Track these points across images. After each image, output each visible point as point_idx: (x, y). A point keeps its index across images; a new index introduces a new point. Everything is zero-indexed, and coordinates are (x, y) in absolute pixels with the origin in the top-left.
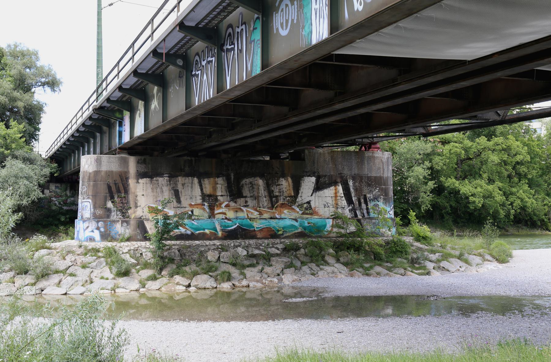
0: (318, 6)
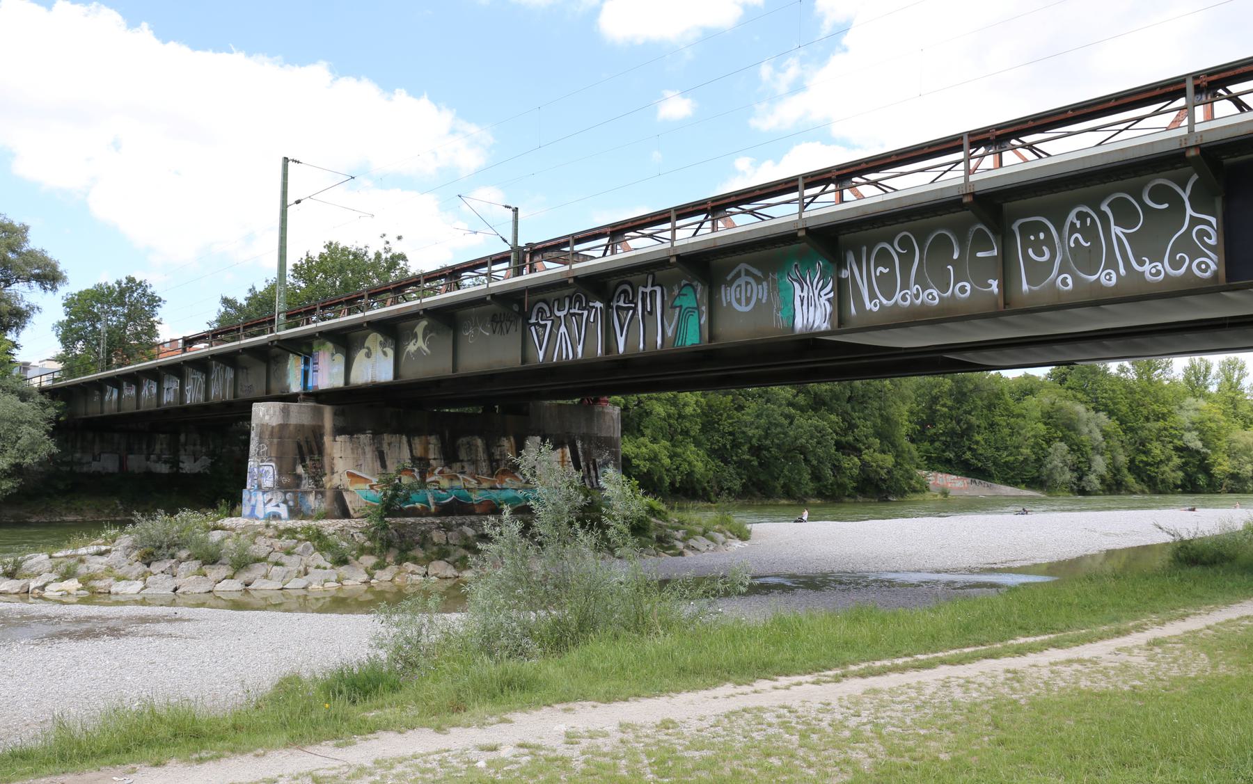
0: (805, 294)
